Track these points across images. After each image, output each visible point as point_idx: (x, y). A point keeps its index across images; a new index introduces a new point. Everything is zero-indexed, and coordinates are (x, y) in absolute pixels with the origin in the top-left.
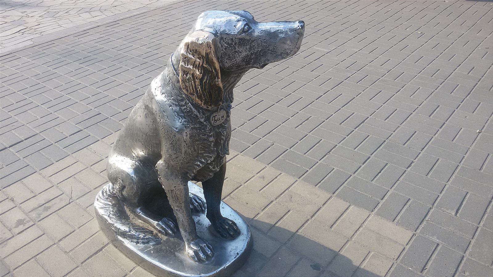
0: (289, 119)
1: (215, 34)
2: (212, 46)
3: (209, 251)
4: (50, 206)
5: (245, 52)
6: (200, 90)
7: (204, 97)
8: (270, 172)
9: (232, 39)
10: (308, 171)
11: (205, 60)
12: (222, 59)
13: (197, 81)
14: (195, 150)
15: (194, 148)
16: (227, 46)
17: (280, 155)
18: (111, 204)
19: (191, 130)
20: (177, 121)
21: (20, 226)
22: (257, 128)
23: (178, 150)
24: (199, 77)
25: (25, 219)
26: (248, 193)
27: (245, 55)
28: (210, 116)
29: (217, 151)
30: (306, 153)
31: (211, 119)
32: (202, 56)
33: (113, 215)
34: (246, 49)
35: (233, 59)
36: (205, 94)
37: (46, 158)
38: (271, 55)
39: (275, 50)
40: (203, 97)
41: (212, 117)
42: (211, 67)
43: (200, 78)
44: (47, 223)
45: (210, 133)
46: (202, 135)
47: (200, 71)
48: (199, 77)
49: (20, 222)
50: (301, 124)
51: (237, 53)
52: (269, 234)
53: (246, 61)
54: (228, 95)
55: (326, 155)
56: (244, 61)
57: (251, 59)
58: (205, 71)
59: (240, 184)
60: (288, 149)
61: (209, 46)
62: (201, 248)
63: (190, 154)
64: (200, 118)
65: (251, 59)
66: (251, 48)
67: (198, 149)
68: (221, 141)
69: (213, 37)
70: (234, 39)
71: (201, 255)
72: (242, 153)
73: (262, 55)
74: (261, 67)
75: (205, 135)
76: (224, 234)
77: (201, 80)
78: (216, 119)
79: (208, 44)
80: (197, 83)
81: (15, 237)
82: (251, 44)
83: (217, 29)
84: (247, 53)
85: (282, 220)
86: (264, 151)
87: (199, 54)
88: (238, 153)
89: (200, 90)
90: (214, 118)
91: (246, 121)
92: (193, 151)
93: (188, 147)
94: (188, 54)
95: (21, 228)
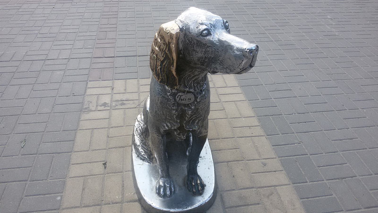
0: (334, 130)
1: (181, 30)
2: (174, 39)
3: (168, 192)
4: (125, 104)
5: (201, 53)
6: (159, 70)
7: (161, 77)
8: (275, 164)
10: (307, 182)
11: (167, 48)
13: (159, 63)
15: (163, 112)
16: (188, 42)
17: (296, 156)
21: (103, 107)
22: (299, 123)
24: (160, 59)
25: (108, 104)
26: (242, 170)
30: (321, 167)
31: (177, 97)
36: (163, 75)
37: (149, 73)
38: (220, 65)
39: (223, 62)
41: (178, 95)
42: (170, 55)
43: (161, 60)
44: (115, 113)
46: (168, 105)
47: (162, 54)
48: (160, 59)
49: (105, 104)
50: (340, 140)
52: (226, 210)
53: (201, 61)
54: (194, 84)
55: (337, 179)
59: (243, 159)
60: (307, 154)
61: (171, 37)
62: (165, 186)
64: (167, 92)
71: (162, 190)
72: (268, 136)
73: (213, 63)
77: (162, 62)
80: (158, 63)
81: (95, 112)
82: (206, 48)
84: (202, 55)
85: (246, 207)
86: (287, 145)
87: (164, 41)
88: (265, 135)
89: (158, 69)
90: (179, 97)
91: (296, 113)
93: (158, 109)
95: (102, 108)
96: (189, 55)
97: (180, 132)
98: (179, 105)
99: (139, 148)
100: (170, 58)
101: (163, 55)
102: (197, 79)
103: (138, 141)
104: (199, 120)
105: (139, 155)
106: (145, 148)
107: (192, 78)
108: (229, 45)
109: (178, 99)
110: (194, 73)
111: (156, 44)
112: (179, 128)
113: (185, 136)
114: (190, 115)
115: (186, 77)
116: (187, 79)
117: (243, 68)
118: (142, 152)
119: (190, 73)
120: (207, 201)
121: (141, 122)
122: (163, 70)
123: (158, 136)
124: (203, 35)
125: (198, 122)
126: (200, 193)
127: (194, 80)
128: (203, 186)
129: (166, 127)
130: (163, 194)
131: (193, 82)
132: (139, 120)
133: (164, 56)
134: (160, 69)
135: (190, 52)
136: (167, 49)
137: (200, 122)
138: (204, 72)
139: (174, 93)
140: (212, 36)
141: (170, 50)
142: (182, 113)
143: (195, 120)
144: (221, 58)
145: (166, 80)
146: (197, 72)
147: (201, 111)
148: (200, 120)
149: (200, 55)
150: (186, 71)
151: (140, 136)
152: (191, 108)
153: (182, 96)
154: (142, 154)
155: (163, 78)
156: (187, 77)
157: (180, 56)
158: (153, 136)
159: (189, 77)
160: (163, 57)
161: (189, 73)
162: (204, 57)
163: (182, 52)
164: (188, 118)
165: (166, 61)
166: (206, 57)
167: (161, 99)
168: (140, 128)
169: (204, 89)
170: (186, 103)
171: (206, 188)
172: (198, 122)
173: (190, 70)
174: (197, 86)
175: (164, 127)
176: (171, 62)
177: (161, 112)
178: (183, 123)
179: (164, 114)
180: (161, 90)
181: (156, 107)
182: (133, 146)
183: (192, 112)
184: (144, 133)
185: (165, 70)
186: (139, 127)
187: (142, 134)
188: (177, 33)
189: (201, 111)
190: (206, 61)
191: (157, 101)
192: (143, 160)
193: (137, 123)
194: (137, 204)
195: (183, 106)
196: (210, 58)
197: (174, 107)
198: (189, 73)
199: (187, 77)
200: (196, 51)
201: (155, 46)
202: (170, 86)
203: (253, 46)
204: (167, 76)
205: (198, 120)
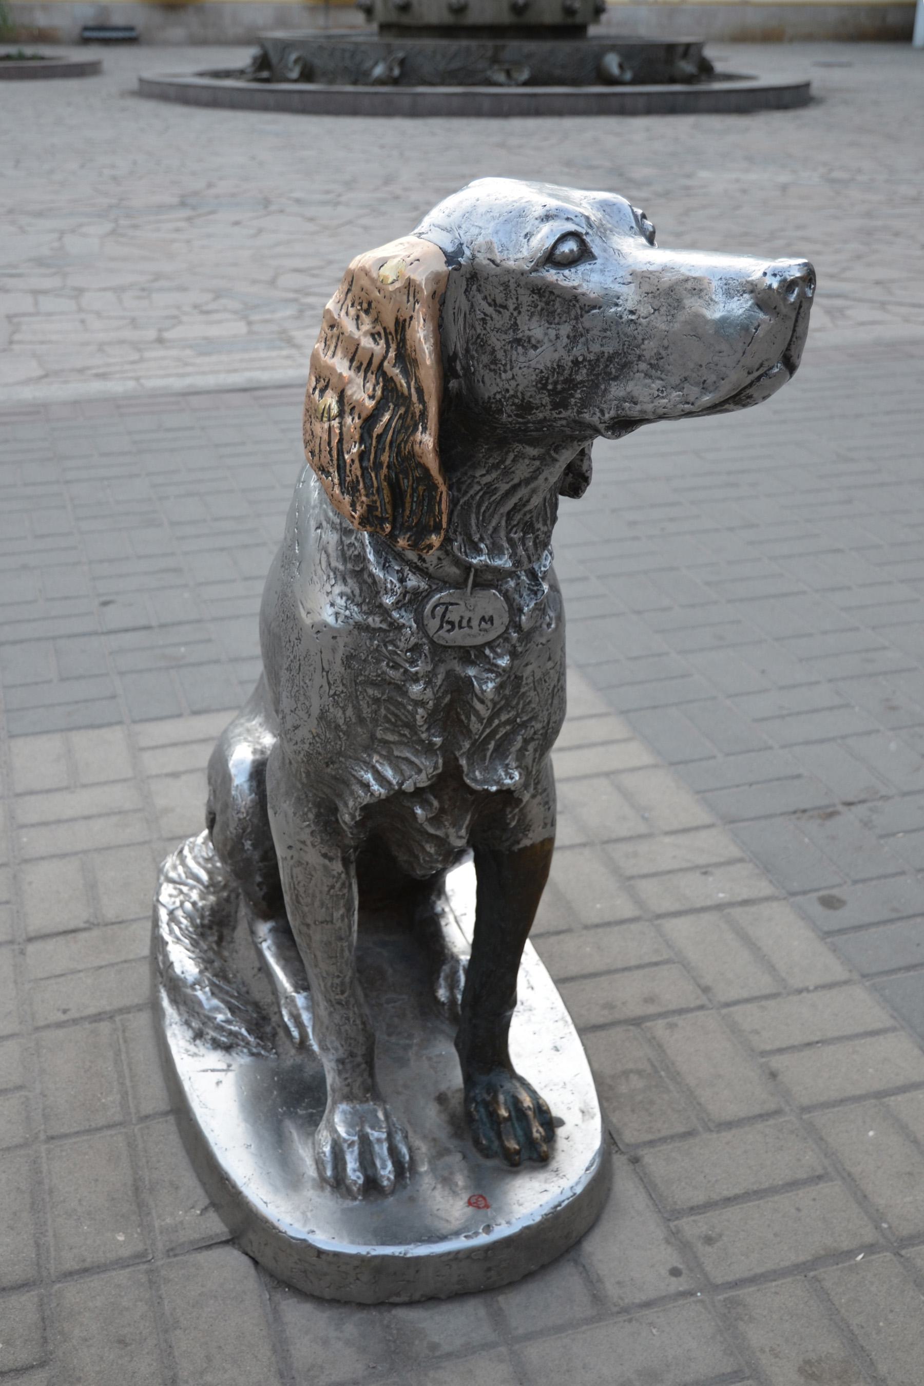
1: (451, 258)
6: (357, 462)
7: (367, 496)
9: (506, 285)
12: (468, 363)
13: (352, 423)
14: (361, 720)
15: (358, 710)
18: (204, 877)
19: (356, 632)
20: (318, 586)
23: (302, 698)
27: (549, 365)
28: (429, 594)
29: (448, 750)
32: (385, 329)
33: (189, 916)
34: (557, 337)
35: (505, 371)
36: (375, 484)
38: (648, 381)
40: (363, 491)
45: (413, 662)
46: (388, 665)
51: (523, 346)
53: (555, 389)
56: (544, 387)
57: (571, 383)
58: (390, 394)
63: (337, 727)
65: (571, 383)
66: (575, 336)
67: (375, 721)
68: (469, 718)
69: (441, 267)
70: (512, 286)
73: (616, 378)
74: (608, 428)
75: (396, 666)
76: (481, 1135)
77: (370, 421)
78: (453, 616)
79: (410, 286)
82: (576, 318)
83: (465, 239)
84: (556, 356)
89: (353, 461)
90: (440, 610)
92: (354, 720)
94: (343, 313)
96: (492, 374)
97: (442, 810)
98: (439, 651)
99: (199, 994)
100: (410, 394)
101: (374, 390)
102: (524, 505)
103: (184, 961)
104: (526, 742)
105: (202, 1032)
106: (227, 993)
107: (498, 503)
108: (687, 280)
109: (433, 625)
110: (513, 472)
111: (336, 347)
112: (438, 785)
113: (463, 832)
114: (490, 705)
115: (472, 497)
116: (479, 506)
117: (761, 365)
118: (217, 1009)
119: (494, 475)
120: (579, 1190)
121: (185, 884)
122: (374, 463)
123: (325, 856)
124: (559, 259)
125: (523, 749)
126: (539, 1156)
127: (509, 513)
128: (551, 1124)
129: (376, 778)
130: (359, 1178)
131: (503, 523)
132: (172, 874)
133: (379, 393)
134: (362, 456)
135: (500, 355)
136: (392, 354)
137: (531, 747)
138: (557, 460)
139: (416, 592)
140: (598, 261)
141: (406, 358)
142: (452, 701)
143: (508, 738)
144: (650, 348)
145: (389, 507)
146: (527, 461)
147: (535, 690)
148: (532, 739)
149: (544, 357)
150: (474, 467)
151: (195, 944)
152: (492, 668)
153: (452, 604)
154: (220, 1017)
155: (375, 502)
156: (478, 498)
157: (451, 385)
158: (299, 863)
159: (488, 496)
160: (372, 397)
161: (488, 479)
162: (570, 364)
163: (459, 367)
164: (480, 719)
165: (390, 412)
166: (580, 359)
167: (346, 640)
168: (188, 905)
169: (545, 572)
170: (469, 642)
171: (561, 1132)
172: (523, 749)
173: (491, 461)
174: (523, 540)
175: (366, 786)
176: (413, 414)
177: (350, 712)
178: (457, 754)
179: (361, 720)
180: (347, 595)
181: (321, 687)
182: (164, 995)
183: (500, 688)
184: (208, 932)
185: (385, 458)
186: (182, 903)
187: (202, 935)
188: (436, 278)
189: (532, 693)
190: (579, 378)
191: (327, 656)
192: (227, 1048)
193: (167, 890)
194: (233, 1261)
195: (456, 661)
196: (598, 360)
197: (417, 666)
198: (488, 479)
199: (478, 498)
200: (529, 341)
201: (330, 353)
202: (408, 536)
203: (792, 266)
204: (391, 485)
205: (520, 738)
